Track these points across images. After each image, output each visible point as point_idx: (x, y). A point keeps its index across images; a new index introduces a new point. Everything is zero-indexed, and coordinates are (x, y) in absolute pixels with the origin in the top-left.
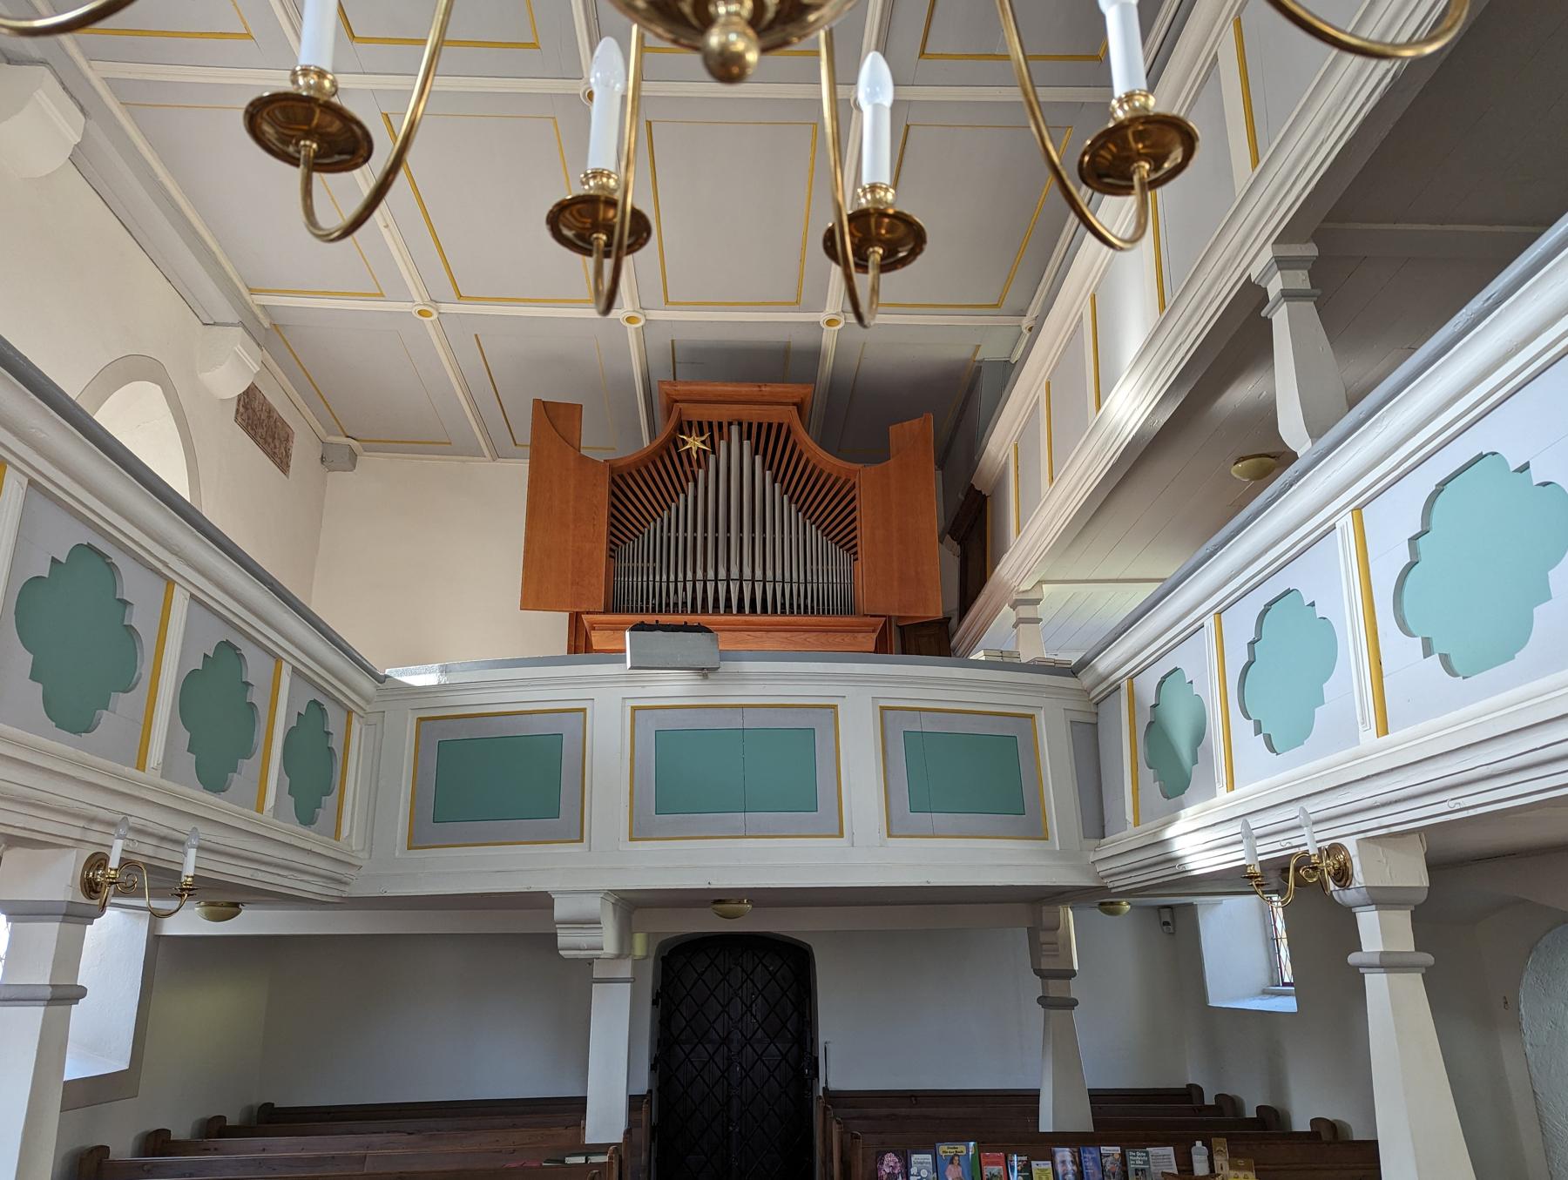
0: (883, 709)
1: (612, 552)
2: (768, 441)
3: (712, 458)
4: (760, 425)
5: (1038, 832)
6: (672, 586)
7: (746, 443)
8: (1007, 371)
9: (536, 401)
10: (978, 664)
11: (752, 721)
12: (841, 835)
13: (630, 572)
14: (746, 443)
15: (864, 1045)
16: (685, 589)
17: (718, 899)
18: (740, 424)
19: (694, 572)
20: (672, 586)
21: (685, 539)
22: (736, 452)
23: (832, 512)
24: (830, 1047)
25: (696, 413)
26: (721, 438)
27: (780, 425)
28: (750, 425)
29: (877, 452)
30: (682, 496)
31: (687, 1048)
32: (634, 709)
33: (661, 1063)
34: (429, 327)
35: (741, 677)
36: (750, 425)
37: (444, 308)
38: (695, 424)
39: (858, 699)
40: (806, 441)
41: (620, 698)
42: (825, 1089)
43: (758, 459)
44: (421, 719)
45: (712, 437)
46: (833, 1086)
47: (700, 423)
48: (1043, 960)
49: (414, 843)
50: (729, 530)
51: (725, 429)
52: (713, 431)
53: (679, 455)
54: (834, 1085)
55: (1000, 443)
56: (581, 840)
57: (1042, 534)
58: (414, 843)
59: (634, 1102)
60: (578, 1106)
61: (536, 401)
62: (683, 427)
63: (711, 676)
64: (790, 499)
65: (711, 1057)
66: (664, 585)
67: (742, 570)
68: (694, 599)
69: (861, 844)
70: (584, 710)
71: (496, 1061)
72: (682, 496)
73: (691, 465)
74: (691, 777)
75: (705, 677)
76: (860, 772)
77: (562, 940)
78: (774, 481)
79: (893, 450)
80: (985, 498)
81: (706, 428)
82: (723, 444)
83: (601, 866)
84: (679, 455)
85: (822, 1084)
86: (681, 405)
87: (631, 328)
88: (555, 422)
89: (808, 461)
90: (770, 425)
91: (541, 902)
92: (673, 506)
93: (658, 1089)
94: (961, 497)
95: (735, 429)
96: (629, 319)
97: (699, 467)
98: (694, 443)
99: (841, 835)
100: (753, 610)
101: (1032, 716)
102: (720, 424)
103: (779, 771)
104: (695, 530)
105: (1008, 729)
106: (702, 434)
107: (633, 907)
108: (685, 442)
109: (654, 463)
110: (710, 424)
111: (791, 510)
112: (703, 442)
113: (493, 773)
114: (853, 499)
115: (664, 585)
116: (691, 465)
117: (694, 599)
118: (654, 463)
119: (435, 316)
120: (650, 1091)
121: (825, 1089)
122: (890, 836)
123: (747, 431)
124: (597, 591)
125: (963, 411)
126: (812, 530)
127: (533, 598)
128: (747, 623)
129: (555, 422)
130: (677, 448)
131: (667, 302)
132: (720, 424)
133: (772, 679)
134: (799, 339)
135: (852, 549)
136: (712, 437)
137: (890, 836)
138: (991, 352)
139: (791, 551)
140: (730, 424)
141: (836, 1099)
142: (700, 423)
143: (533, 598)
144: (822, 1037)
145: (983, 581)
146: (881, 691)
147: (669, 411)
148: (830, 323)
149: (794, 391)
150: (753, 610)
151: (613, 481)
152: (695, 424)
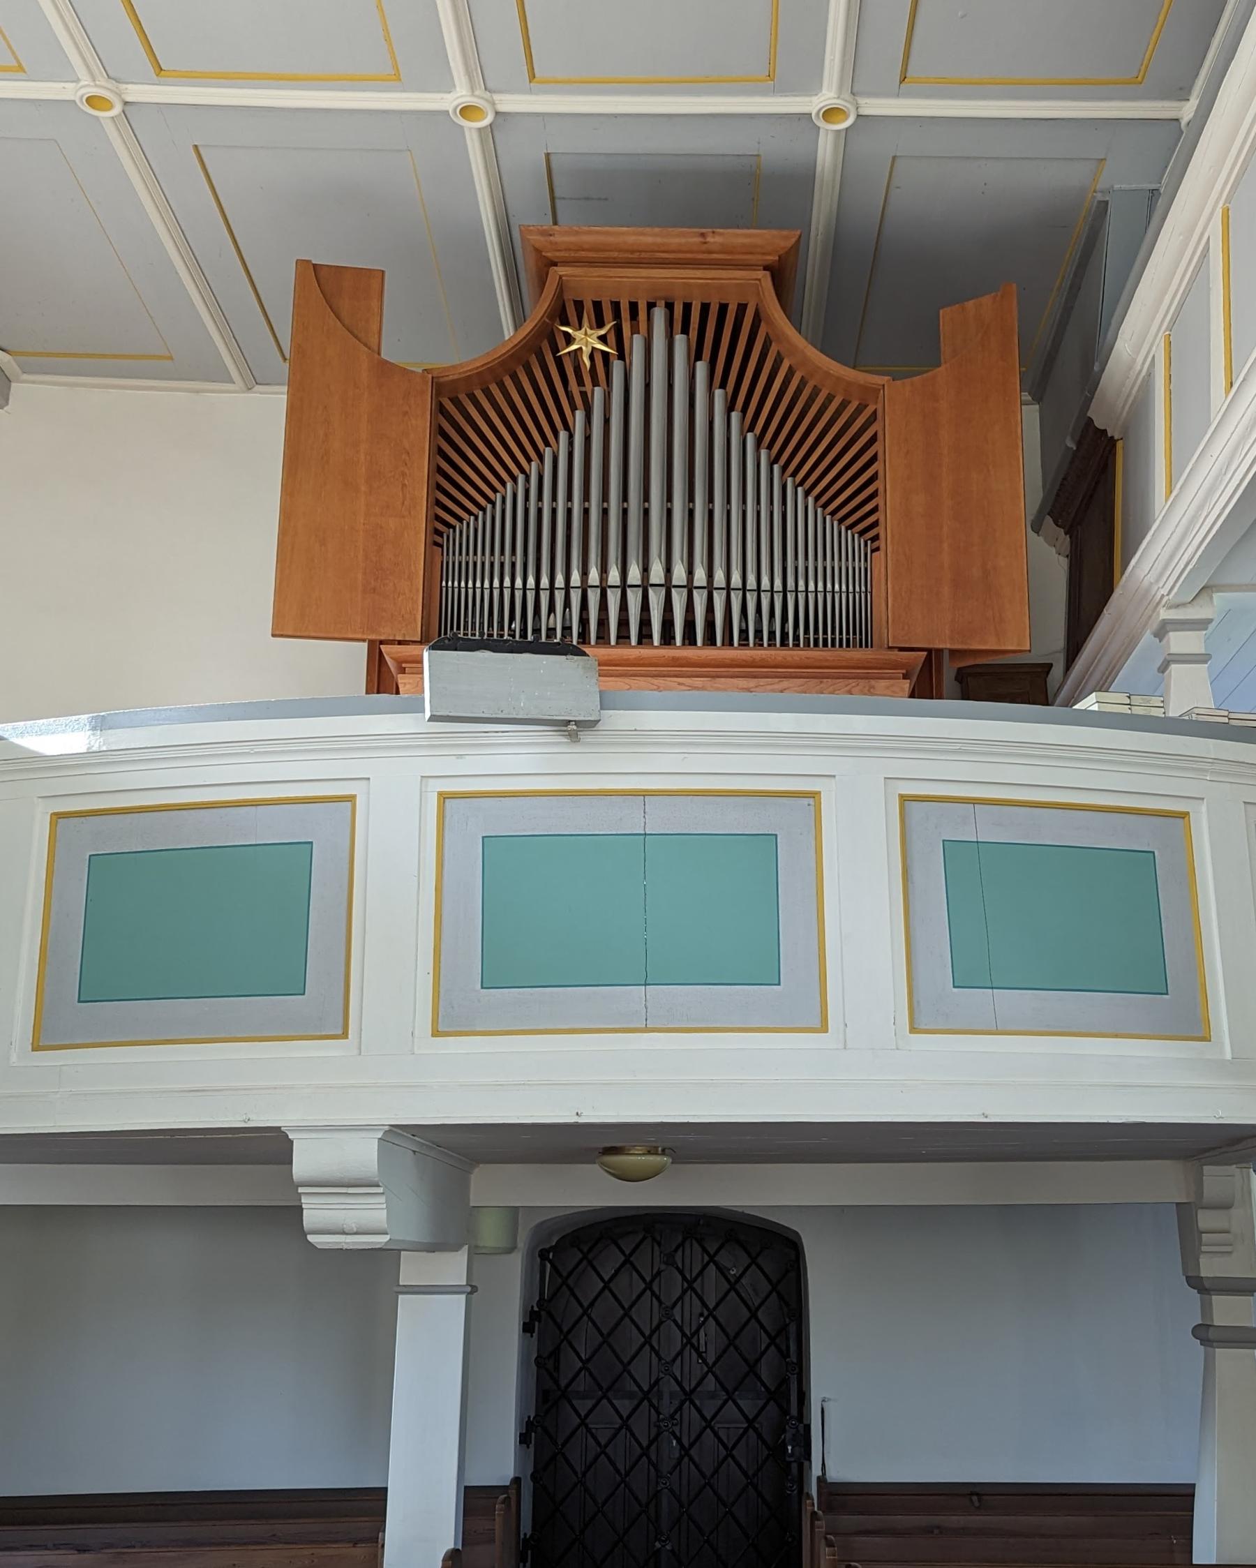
0: (904, 799)
1: (439, 531)
2: (721, 336)
3: (617, 367)
4: (705, 308)
5: (1194, 1027)
6: (544, 597)
7: (718, 393)
8: (1152, 205)
9: (302, 264)
10: (1090, 720)
11: (659, 819)
12: (824, 1028)
13: (466, 571)
14: (680, 339)
15: (892, 1403)
16: (567, 604)
17: (601, 1145)
18: (670, 306)
19: (585, 573)
20: (544, 597)
21: (569, 512)
22: (660, 353)
23: (834, 466)
24: (829, 1408)
25: (590, 282)
26: (635, 330)
27: (742, 308)
28: (687, 307)
29: (919, 351)
30: (563, 435)
31: (583, 1406)
32: (444, 797)
33: (536, 1431)
34: (110, 129)
35: (639, 739)
36: (687, 307)
37: (137, 92)
38: (588, 306)
39: (856, 780)
40: (798, 346)
41: (410, 779)
42: (822, 1480)
43: (701, 368)
44: (58, 816)
45: (618, 330)
46: (834, 1475)
47: (597, 306)
48: (1203, 1260)
49: (45, 1038)
50: (646, 497)
51: (642, 315)
52: (618, 317)
53: (559, 362)
54: (836, 1474)
55: (1139, 337)
56: (345, 1035)
57: (1211, 491)
58: (45, 1038)
59: (475, 1501)
60: (372, 1503)
61: (302, 264)
62: (565, 311)
63: (586, 737)
64: (759, 441)
65: (625, 1423)
66: (531, 596)
67: (669, 573)
68: (584, 622)
69: (855, 1040)
70: (351, 799)
71: (238, 1431)
72: (563, 435)
73: (581, 382)
74: (541, 920)
75: (574, 737)
76: (861, 913)
77: (311, 1217)
78: (730, 408)
79: (946, 350)
80: (1112, 442)
81: (608, 313)
82: (637, 343)
83: (362, 1080)
84: (559, 362)
85: (816, 1471)
86: (562, 270)
87: (471, 127)
88: (335, 297)
89: (803, 382)
90: (723, 308)
91: (271, 1147)
92: (548, 453)
93: (534, 1477)
94: (1071, 445)
95: (659, 315)
96: (466, 111)
97: (595, 383)
98: (586, 340)
99: (824, 1028)
100: (690, 638)
101: (1184, 816)
102: (634, 307)
103: (716, 913)
104: (586, 496)
105: (1138, 837)
106: (600, 325)
107: (451, 1155)
108: (569, 339)
109: (515, 378)
110: (616, 306)
111: (758, 460)
112: (603, 339)
113: (185, 915)
114: (873, 439)
115: (531, 596)
116: (581, 382)
117: (584, 622)
118: (515, 378)
119: (117, 109)
120: (517, 1481)
121: (822, 1480)
122: (913, 1030)
123: (682, 317)
124: (408, 605)
125: (1075, 288)
126: (799, 500)
127: (297, 616)
128: (676, 662)
129: (335, 297)
130: (555, 349)
131: (532, 76)
132: (634, 307)
133: (693, 746)
134: (775, 149)
135: (869, 531)
136: (618, 330)
137: (913, 1030)
138: (1120, 178)
139: (762, 541)
140: (651, 306)
141: (840, 1496)
142: (597, 306)
143: (297, 616)
144: (818, 1389)
145: (1106, 589)
146: (898, 767)
147: (542, 282)
148: (830, 114)
149: (771, 240)
150: (690, 638)
151: (442, 409)
152: (588, 306)
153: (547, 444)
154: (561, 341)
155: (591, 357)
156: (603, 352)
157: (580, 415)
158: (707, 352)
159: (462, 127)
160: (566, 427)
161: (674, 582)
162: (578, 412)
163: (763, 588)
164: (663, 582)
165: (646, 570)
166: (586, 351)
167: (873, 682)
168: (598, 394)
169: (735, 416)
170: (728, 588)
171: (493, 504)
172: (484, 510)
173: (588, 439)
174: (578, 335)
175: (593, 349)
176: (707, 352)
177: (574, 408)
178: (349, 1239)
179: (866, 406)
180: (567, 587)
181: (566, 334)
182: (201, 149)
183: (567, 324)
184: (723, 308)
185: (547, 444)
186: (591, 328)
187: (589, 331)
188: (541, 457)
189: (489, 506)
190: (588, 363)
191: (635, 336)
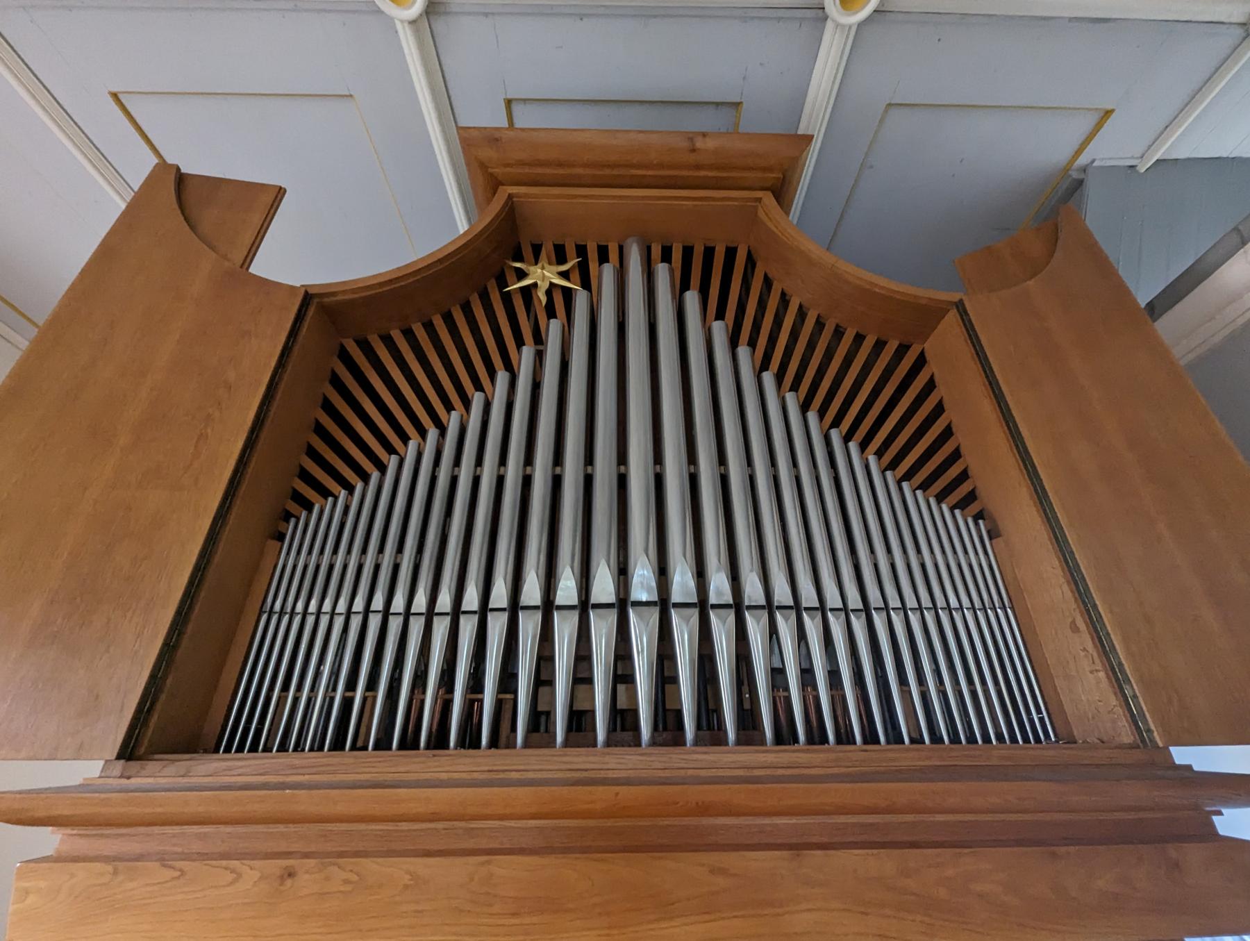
3: (581, 301)
14: (662, 271)
53: (507, 299)
72: (502, 377)
78: (734, 343)
81: (571, 251)
84: (507, 299)
90: (709, 252)
112: (565, 275)
130: (502, 282)
153: (479, 387)
154: (510, 276)
155: (549, 293)
156: (564, 288)
157: (528, 352)
158: (696, 278)
159: (392, 19)
160: (509, 367)
161: (713, 600)
162: (525, 349)
163: (676, 597)
164: (695, 600)
165: (623, 573)
166: (543, 286)
167: (1172, 851)
168: (554, 329)
169: (743, 351)
170: (703, 605)
171: (382, 468)
172: (365, 477)
173: (536, 387)
174: (532, 269)
175: (551, 284)
176: (696, 278)
177: (520, 343)
178: (829, 63)
179: (908, 347)
180: (514, 607)
181: (517, 269)
182: (121, 96)
183: (521, 260)
184: (709, 252)
185: (479, 387)
186: (550, 264)
187: (546, 265)
188: (467, 403)
189: (375, 475)
190: (544, 299)
191: (606, 265)
